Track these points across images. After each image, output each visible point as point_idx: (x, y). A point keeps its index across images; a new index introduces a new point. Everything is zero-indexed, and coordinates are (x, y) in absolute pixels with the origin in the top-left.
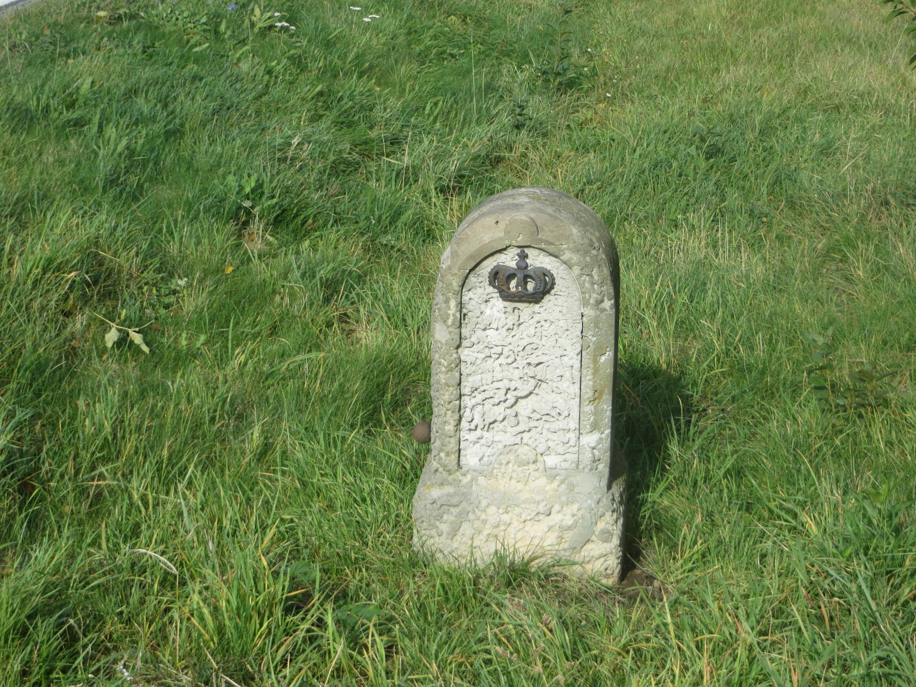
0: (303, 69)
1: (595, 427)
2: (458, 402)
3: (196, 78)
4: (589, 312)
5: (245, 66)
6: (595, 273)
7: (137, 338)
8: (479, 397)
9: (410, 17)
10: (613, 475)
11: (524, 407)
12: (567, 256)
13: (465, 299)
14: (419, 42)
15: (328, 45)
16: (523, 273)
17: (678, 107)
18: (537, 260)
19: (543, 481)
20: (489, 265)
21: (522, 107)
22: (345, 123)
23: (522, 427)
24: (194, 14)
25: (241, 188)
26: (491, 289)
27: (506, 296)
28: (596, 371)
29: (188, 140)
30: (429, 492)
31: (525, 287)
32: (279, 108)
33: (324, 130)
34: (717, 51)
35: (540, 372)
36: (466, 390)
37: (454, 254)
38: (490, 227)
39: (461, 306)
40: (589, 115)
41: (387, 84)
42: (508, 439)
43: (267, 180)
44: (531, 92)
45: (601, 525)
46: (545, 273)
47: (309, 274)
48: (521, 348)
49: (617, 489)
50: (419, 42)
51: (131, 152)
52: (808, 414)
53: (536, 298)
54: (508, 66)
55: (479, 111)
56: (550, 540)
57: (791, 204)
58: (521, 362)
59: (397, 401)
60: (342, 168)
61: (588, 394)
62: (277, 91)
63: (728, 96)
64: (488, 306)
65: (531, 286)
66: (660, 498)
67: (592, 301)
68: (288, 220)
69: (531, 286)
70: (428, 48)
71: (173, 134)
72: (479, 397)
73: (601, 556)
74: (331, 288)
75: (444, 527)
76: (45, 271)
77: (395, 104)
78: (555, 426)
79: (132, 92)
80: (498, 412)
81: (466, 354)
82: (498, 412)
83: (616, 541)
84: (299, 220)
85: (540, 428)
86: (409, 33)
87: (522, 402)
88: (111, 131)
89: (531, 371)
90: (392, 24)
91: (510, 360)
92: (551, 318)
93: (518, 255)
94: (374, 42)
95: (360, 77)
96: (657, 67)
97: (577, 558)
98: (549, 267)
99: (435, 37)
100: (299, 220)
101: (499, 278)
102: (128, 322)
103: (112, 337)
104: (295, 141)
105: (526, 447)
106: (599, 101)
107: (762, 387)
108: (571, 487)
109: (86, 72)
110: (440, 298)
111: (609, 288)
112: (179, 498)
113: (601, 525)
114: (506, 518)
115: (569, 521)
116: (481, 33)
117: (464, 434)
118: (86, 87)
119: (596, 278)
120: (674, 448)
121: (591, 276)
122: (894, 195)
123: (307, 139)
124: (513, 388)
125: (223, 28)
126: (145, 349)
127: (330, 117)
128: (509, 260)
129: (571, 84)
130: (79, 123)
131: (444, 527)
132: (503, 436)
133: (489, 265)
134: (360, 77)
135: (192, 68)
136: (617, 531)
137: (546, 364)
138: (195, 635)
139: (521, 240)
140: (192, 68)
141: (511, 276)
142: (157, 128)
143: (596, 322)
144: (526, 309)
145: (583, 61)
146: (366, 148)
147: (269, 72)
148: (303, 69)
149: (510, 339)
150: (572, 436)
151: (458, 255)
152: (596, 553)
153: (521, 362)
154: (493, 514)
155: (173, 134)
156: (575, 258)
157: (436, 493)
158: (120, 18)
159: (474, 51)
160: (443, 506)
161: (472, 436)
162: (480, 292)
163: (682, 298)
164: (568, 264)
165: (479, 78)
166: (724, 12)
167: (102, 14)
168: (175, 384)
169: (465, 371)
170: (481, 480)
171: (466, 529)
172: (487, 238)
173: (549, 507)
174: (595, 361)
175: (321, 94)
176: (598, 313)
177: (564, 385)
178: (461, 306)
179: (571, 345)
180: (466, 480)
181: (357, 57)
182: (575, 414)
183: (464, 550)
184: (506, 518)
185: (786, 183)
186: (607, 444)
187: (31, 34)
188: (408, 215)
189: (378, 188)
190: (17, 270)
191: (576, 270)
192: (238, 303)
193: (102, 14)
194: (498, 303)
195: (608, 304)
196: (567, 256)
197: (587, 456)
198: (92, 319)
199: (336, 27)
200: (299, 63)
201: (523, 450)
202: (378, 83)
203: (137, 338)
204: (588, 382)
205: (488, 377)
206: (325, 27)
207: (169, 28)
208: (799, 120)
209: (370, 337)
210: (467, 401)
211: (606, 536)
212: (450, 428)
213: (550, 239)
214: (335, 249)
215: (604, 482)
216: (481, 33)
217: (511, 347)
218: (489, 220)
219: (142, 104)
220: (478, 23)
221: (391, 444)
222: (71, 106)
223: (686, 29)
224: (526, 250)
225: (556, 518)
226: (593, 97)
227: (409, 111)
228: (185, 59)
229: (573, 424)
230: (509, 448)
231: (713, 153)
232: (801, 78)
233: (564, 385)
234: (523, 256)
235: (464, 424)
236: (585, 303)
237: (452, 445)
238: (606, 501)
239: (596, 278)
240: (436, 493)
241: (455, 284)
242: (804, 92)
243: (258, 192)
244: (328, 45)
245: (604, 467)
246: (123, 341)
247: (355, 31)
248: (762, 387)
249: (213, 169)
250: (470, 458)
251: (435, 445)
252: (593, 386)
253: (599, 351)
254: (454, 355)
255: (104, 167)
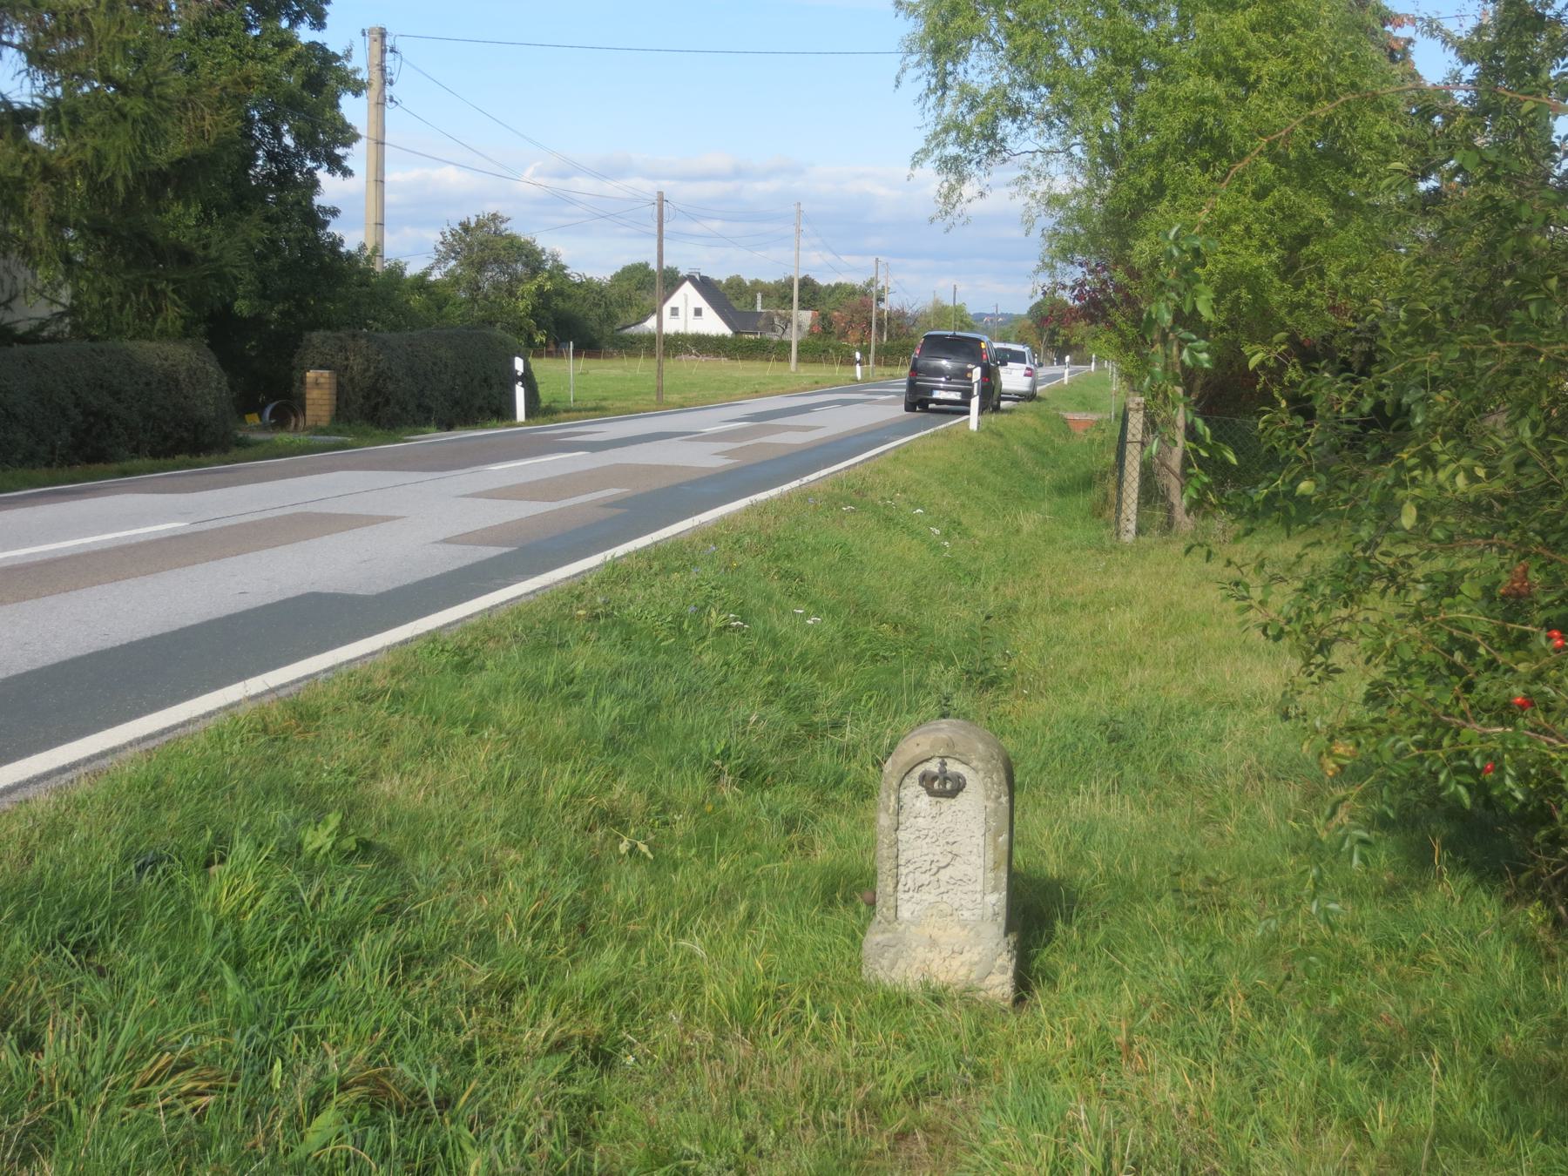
0: (754, 662)
1: (995, 889)
3: (667, 666)
4: (991, 805)
5: (706, 658)
7: (644, 848)
8: (911, 867)
9: (847, 623)
10: (1009, 929)
11: (944, 875)
12: (974, 764)
14: (856, 645)
15: (775, 644)
16: (944, 776)
17: (1092, 702)
18: (954, 767)
19: (957, 929)
20: (919, 770)
21: (947, 699)
22: (793, 707)
24: (660, 614)
25: (713, 750)
27: (932, 793)
28: (996, 848)
29: (664, 715)
30: (874, 938)
31: (945, 787)
32: (738, 692)
33: (776, 712)
34: (1128, 658)
35: (955, 848)
36: (902, 862)
37: (894, 763)
38: (924, 742)
39: (899, 800)
40: (1008, 708)
41: (827, 680)
42: (932, 898)
43: (733, 744)
44: (957, 687)
45: (999, 962)
46: (959, 776)
47: (772, 812)
49: (1012, 938)
50: (856, 645)
51: (622, 719)
52: (1165, 909)
53: (952, 794)
54: (936, 668)
55: (909, 703)
56: (963, 972)
57: (1180, 778)
58: (942, 842)
59: (852, 891)
60: (790, 742)
61: (991, 864)
62: (734, 679)
63: (1134, 694)
64: (918, 800)
65: (948, 786)
66: (1047, 957)
68: (751, 775)
69: (948, 786)
70: (863, 651)
71: (653, 708)
72: (911, 867)
73: (1000, 985)
74: (790, 824)
75: (885, 963)
76: (572, 795)
77: (835, 695)
78: (966, 889)
79: (616, 674)
80: (926, 878)
81: (902, 835)
82: (926, 878)
83: (1010, 974)
84: (760, 777)
86: (846, 637)
87: (942, 872)
88: (606, 702)
89: (949, 848)
90: (831, 628)
94: (815, 644)
95: (804, 671)
96: (1072, 669)
97: (983, 986)
99: (870, 641)
100: (760, 777)
101: (927, 780)
102: (637, 836)
103: (624, 848)
104: (753, 718)
106: (1017, 697)
107: (1130, 893)
108: (978, 935)
109: (581, 659)
110: (883, 795)
111: (1005, 788)
113: (999, 962)
114: (930, 955)
115: (976, 958)
116: (912, 638)
117: (900, 895)
118: (580, 668)
120: (1059, 925)
122: (1267, 771)
123: (761, 718)
125: (685, 626)
126: (650, 856)
127: (780, 703)
128: (933, 767)
129: (992, 683)
130: (578, 696)
131: (885, 963)
132: (928, 896)
133: (919, 770)
134: (804, 671)
135: (662, 658)
136: (1011, 966)
139: (942, 752)
140: (662, 658)
141: (935, 778)
142: (641, 702)
143: (995, 811)
144: (946, 802)
145: (1001, 663)
146: (811, 729)
147: (727, 663)
148: (754, 662)
150: (979, 896)
152: (996, 982)
153: (942, 842)
154: (921, 953)
155: (653, 708)
156: (980, 765)
157: (879, 938)
158: (597, 617)
159: (905, 654)
160: (886, 946)
161: (906, 896)
162: (913, 789)
163: (1078, 837)
165: (909, 677)
166: (1137, 624)
167: (581, 612)
168: (677, 878)
169: (901, 848)
170: (913, 928)
171: (901, 964)
172: (917, 751)
174: (995, 841)
175: (771, 683)
177: (973, 858)
178: (899, 800)
179: (977, 828)
180: (901, 928)
181: (801, 655)
182: (981, 879)
183: (898, 979)
184: (930, 955)
185: (1176, 763)
186: (1004, 902)
187: (525, 627)
188: (850, 779)
189: (825, 759)
190: (552, 795)
191: (981, 774)
192: (714, 832)
193: (581, 612)
194: (926, 798)
195: (1004, 799)
196: (974, 764)
197: (990, 911)
198: (608, 835)
199: (782, 629)
200: (752, 658)
201: (943, 906)
202: (819, 678)
203: (644, 848)
204: (990, 855)
205: (918, 852)
206: (772, 629)
207: (640, 625)
208: (1194, 713)
209: (823, 855)
210: (903, 870)
211: (1003, 970)
212: (890, 889)
214: (789, 798)
215: (1002, 930)
216: (912, 638)
218: (919, 739)
219: (625, 684)
220: (908, 630)
221: (843, 916)
222: (570, 682)
223: (1099, 638)
225: (966, 956)
226: (1012, 695)
227: (844, 703)
228: (656, 650)
229: (979, 888)
230: (932, 905)
231: (1115, 738)
232: (1201, 680)
233: (973, 858)
234: (944, 764)
235: (900, 887)
236: (988, 798)
237: (891, 902)
238: (1003, 944)
240: (879, 938)
241: (895, 784)
242: (1203, 692)
243: (726, 755)
244: (775, 644)
245: (1001, 920)
246: (633, 850)
247: (798, 633)
248: (1130, 893)
249: (687, 736)
250: (905, 913)
251: (879, 903)
253: (998, 834)
255: (604, 728)
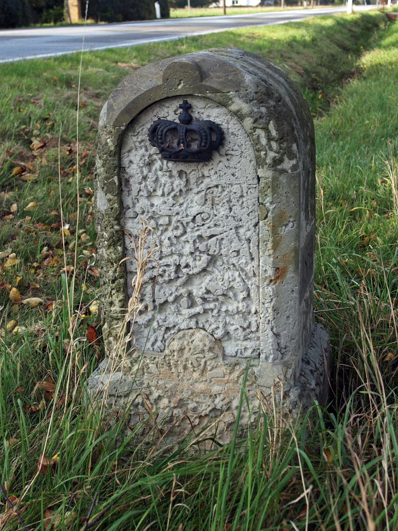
2: (122, 281)
4: (265, 173)
6: (271, 126)
11: (198, 289)
13: (125, 161)
18: (206, 113)
23: (198, 309)
26: (154, 150)
37: (110, 108)
48: (190, 218)
67: (268, 161)
85: (215, 311)
91: (179, 232)
92: (222, 182)
93: (181, 107)
98: (218, 121)
101: (157, 135)
105: (203, 332)
112: (384, 299)
119: (274, 133)
121: (266, 129)
124: (183, 265)
128: (170, 113)
137: (219, 237)
138: (20, 471)
143: (274, 186)
144: (193, 171)
149: (176, 208)
151: (113, 110)
156: (245, 108)
164: (239, 116)
173: (227, 400)
176: (277, 174)
191: (248, 122)
213: (215, 86)
217: (179, 217)
224: (189, 101)
234: (187, 108)
236: (260, 162)
239: (274, 133)
252: (274, 263)
253: (279, 221)
254: (117, 227)
